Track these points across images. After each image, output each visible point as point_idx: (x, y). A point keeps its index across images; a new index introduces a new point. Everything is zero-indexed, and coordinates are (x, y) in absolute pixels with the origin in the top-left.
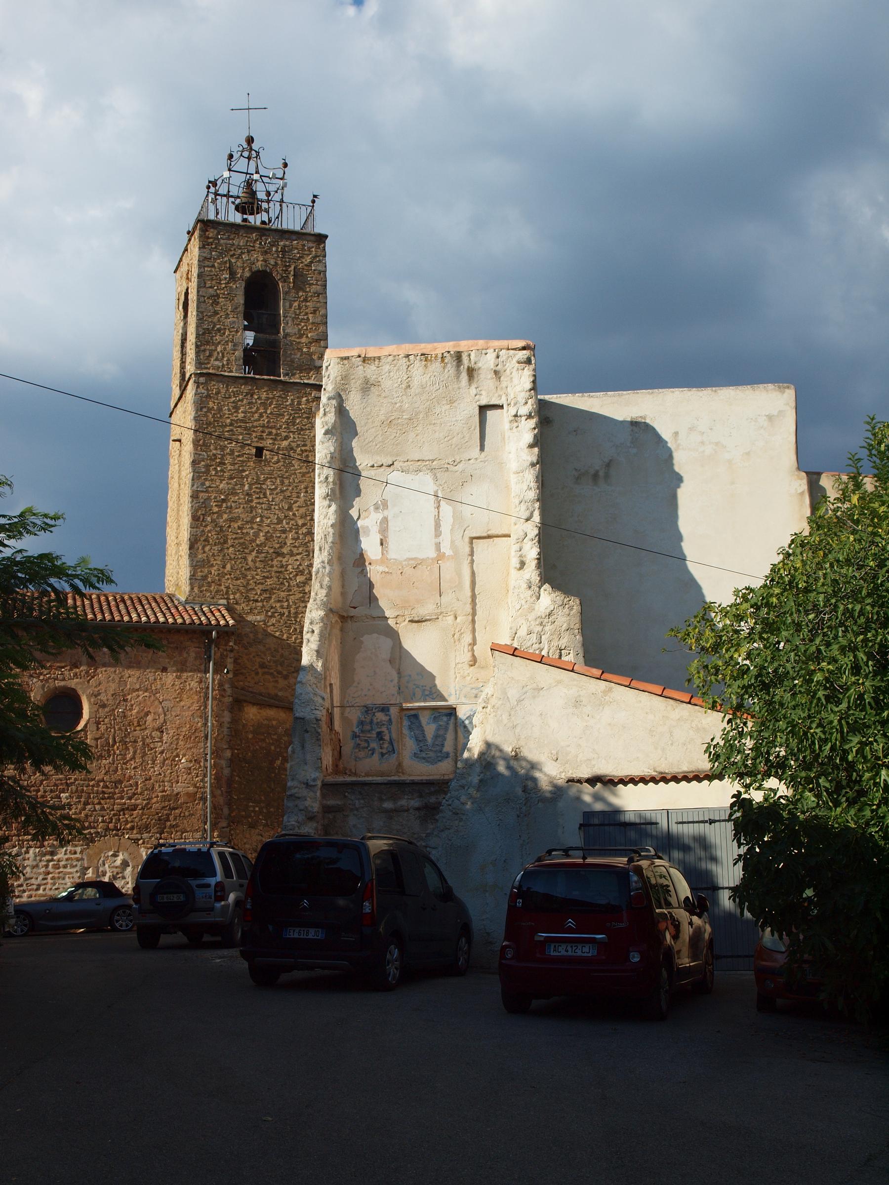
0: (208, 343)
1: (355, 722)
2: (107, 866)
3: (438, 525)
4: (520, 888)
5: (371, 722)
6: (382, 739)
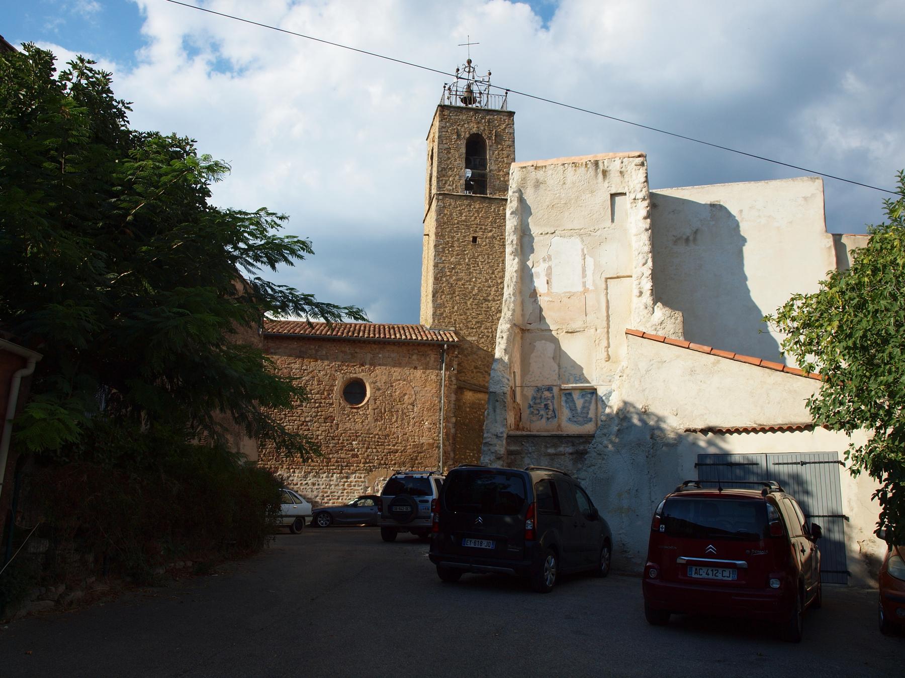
0: (444, 176)
1: (530, 397)
3: (584, 271)
4: (662, 514)
5: (541, 398)
6: (547, 408)
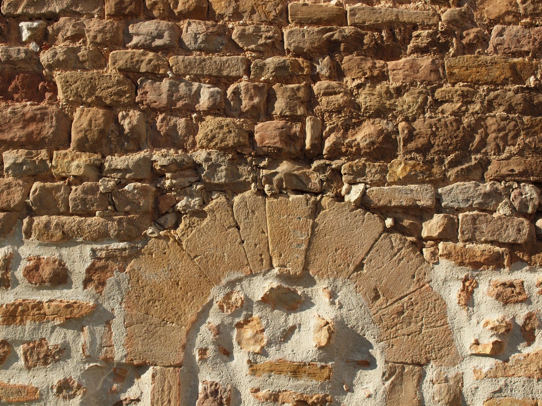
2: (240, 359)
